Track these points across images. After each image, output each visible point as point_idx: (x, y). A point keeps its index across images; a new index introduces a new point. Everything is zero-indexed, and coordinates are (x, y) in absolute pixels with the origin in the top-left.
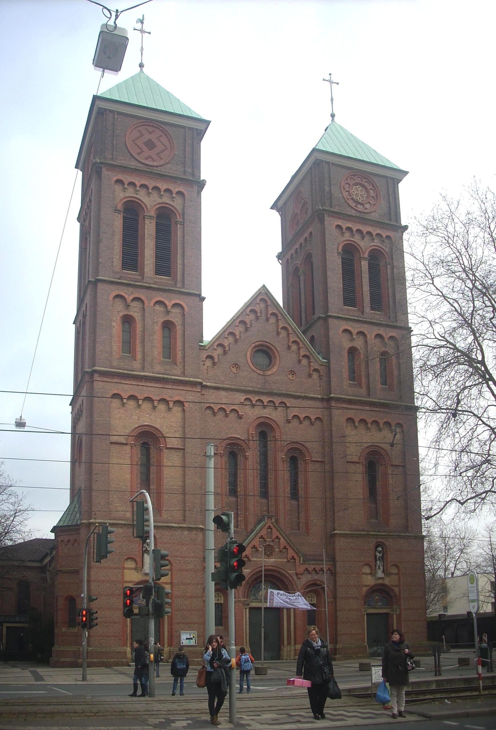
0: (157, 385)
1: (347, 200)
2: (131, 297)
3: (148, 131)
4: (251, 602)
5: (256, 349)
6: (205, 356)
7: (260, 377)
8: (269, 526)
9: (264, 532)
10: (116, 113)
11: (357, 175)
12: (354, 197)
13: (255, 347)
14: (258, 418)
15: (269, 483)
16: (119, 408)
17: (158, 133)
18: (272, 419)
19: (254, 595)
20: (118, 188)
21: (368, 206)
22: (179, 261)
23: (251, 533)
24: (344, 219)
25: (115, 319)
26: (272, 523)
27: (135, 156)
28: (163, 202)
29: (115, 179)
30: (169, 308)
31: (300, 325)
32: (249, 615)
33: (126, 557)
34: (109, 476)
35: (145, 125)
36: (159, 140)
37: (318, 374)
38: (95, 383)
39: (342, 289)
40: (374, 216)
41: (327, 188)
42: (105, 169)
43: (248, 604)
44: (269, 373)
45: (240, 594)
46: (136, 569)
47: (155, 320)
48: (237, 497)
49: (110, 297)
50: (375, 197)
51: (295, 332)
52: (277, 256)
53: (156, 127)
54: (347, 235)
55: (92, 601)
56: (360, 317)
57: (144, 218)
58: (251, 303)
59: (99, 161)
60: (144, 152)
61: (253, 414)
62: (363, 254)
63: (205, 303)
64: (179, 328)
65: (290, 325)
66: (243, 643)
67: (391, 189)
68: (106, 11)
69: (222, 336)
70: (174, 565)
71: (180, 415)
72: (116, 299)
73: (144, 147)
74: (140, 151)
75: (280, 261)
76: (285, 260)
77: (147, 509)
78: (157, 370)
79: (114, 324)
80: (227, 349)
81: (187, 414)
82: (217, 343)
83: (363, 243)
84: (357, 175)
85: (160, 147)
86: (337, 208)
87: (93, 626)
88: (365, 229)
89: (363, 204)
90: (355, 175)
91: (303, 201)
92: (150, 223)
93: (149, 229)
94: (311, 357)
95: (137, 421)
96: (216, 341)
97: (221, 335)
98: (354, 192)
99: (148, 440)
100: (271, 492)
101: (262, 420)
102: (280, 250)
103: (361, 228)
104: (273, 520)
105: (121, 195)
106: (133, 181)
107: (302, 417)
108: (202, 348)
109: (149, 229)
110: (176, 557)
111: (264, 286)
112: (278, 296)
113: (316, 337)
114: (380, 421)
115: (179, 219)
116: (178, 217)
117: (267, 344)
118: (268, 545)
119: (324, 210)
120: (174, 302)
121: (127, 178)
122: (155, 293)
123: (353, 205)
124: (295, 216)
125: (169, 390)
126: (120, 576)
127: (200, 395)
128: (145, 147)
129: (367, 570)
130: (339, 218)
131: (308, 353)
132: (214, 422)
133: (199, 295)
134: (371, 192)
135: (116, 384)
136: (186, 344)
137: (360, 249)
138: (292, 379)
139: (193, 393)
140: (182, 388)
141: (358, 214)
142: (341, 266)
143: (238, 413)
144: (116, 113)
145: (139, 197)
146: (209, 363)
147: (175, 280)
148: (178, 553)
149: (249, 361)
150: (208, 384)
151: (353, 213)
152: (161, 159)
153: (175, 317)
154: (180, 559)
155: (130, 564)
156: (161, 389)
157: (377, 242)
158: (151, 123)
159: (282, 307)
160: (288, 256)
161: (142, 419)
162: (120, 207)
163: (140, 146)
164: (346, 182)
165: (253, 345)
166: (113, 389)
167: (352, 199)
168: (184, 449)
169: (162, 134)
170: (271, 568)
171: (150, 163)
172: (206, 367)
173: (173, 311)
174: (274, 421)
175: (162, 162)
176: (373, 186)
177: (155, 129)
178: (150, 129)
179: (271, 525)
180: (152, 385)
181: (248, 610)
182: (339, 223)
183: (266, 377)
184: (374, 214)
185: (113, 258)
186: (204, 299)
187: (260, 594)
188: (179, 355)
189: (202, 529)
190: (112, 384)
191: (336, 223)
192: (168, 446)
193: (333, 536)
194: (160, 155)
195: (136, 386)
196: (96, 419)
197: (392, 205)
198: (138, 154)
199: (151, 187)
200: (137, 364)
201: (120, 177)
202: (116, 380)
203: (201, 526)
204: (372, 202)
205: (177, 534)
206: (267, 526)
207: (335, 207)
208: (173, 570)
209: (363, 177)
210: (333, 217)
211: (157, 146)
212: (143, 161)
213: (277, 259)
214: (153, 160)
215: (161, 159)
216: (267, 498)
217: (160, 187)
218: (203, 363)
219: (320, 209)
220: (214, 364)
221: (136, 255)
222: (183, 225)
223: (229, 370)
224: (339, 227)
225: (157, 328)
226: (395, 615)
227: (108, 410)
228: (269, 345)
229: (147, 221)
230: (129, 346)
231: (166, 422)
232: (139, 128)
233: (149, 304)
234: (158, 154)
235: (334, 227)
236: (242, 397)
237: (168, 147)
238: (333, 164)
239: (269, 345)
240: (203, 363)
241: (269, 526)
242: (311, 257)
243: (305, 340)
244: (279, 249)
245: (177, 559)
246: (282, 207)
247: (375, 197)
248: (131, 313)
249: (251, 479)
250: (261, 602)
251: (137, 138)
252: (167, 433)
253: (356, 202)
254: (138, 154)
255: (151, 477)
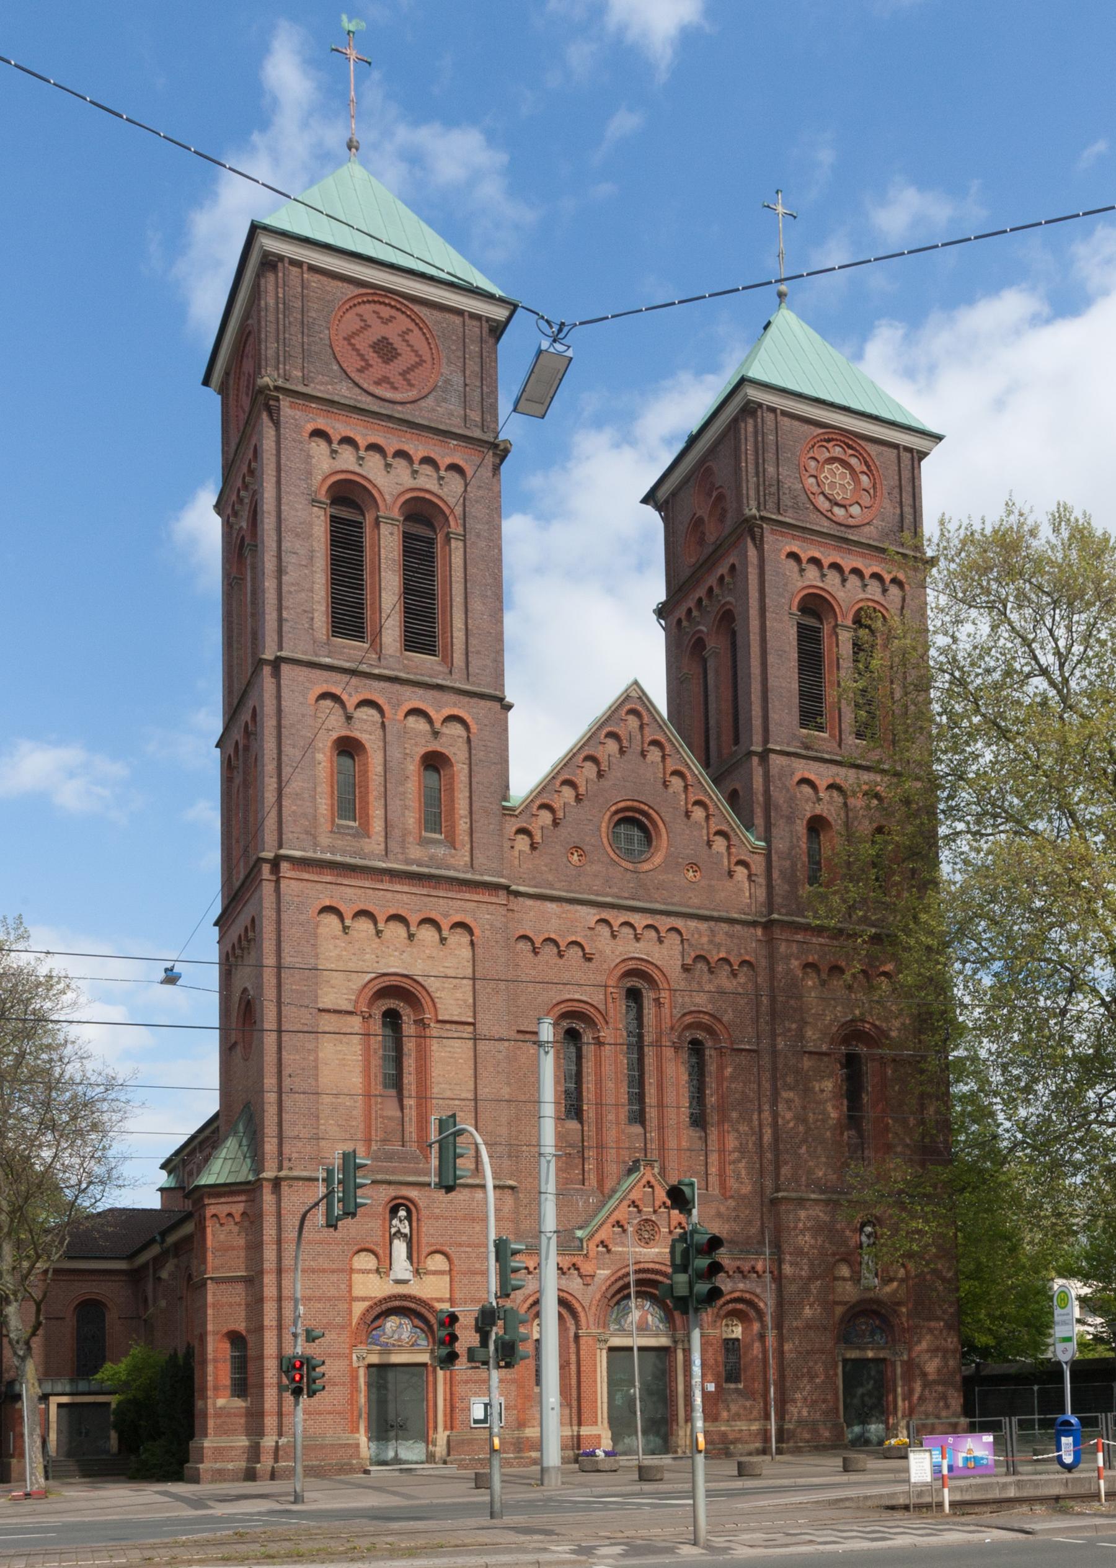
0: (414, 890)
1: (811, 496)
2: (355, 700)
3: (380, 318)
4: (612, 1335)
5: (620, 815)
6: (514, 829)
7: (629, 875)
8: (649, 1182)
9: (635, 1195)
10: (305, 268)
11: (833, 440)
12: (827, 491)
13: (616, 812)
14: (624, 961)
15: (647, 1095)
16: (335, 938)
17: (403, 322)
18: (652, 964)
19: (618, 1321)
20: (319, 448)
21: (855, 510)
22: (458, 623)
23: (610, 1197)
24: (804, 540)
25: (321, 745)
26: (654, 1175)
27: (352, 375)
28: (418, 486)
29: (310, 427)
30: (437, 725)
31: (707, 765)
32: (608, 1363)
33: (356, 1248)
34: (317, 1080)
35: (374, 302)
36: (404, 340)
37: (746, 871)
38: (283, 884)
39: (797, 692)
40: (867, 535)
41: (771, 470)
42: (287, 404)
43: (606, 1341)
44: (646, 867)
45: (591, 1319)
46: (377, 1271)
47: (408, 751)
48: (581, 1122)
49: (309, 696)
50: (872, 491)
51: (700, 782)
52: (654, 611)
53: (398, 309)
54: (812, 573)
55: (313, 1341)
56: (837, 754)
57: (377, 523)
58: (609, 717)
59: (271, 384)
60: (371, 366)
61: (616, 950)
62: (844, 617)
63: (511, 714)
64: (460, 770)
65: (689, 768)
66: (596, 1418)
67: (906, 474)
68: (542, 323)
69: (549, 787)
70: (456, 1262)
71: (466, 953)
72: (321, 702)
73: (371, 356)
74: (363, 364)
75: (663, 622)
76: (674, 619)
77: (775, 1385)
78: (416, 856)
79: (320, 756)
80: (560, 814)
81: (479, 951)
82: (538, 803)
83: (842, 594)
84: (833, 440)
85: (407, 358)
86: (790, 513)
87: (314, 1393)
88: (848, 562)
89: (844, 506)
90: (829, 441)
91: (715, 494)
92: (391, 534)
93: (387, 547)
94: (732, 834)
95: (376, 965)
96: (536, 797)
97: (546, 786)
98: (826, 478)
99: (396, 1005)
100: (652, 1113)
101: (632, 965)
102: (663, 598)
103: (839, 561)
104: (656, 1170)
105: (325, 465)
106: (352, 435)
107: (714, 957)
108: (508, 812)
109: (387, 547)
110: (460, 1245)
111: (636, 683)
112: (659, 698)
113: (741, 794)
114: (342, 908)
115: (455, 527)
116: (452, 523)
117: (642, 806)
118: (646, 1220)
119: (762, 518)
120: (447, 712)
121: (338, 427)
122: (407, 691)
123: (822, 503)
124: (697, 523)
125: (441, 901)
126: (343, 1286)
127: (504, 912)
128: (375, 355)
129: (845, 1271)
130: (794, 537)
131: (725, 828)
132: (534, 968)
133: (501, 700)
134: (864, 479)
135: (329, 886)
136: (474, 805)
137: (836, 607)
138: (694, 880)
139: (492, 908)
140: (467, 896)
141: (835, 530)
142: (795, 643)
143: (583, 949)
144: (305, 268)
145: (364, 473)
146: (523, 842)
147: (448, 660)
148: (464, 1238)
149: (605, 840)
150: (522, 889)
151: (825, 526)
152: (411, 385)
153: (452, 741)
154: (468, 1249)
155: (366, 1261)
156: (423, 898)
157: (874, 590)
158: (386, 296)
159: (665, 716)
160: (681, 612)
161: (384, 961)
162: (322, 496)
163: (362, 352)
164: (811, 454)
165: (613, 808)
166: (321, 896)
167: (822, 493)
168: (473, 1024)
169: (412, 326)
170: (651, 1266)
171: (389, 395)
172: (516, 854)
173: (445, 730)
174: (657, 966)
175: (412, 394)
176: (868, 467)
177: (393, 312)
178: (386, 312)
179: (652, 1180)
180: (406, 889)
181: (604, 1352)
182: (795, 549)
183: (641, 876)
184: (866, 529)
185: (312, 611)
186: (509, 707)
187: (629, 1319)
188: (463, 825)
189: (512, 1188)
190: (319, 886)
191: (788, 549)
192: (440, 1018)
193: (774, 1202)
194: (408, 376)
195: (371, 891)
196: (289, 959)
197: (907, 510)
198: (359, 370)
199: (390, 451)
200: (374, 844)
201: (321, 423)
202: (329, 879)
203: (511, 1183)
204: (866, 500)
205: (462, 1198)
206: (644, 1181)
207: (785, 511)
208: (454, 1273)
209: (846, 444)
210: (782, 534)
211: (400, 355)
212: (373, 389)
213: (655, 617)
214: (396, 389)
215: (411, 385)
216: (580, 1120)
217: (411, 453)
218: (509, 844)
219: (754, 517)
220: (533, 847)
221: (361, 606)
222: (464, 541)
223: (565, 860)
224: (793, 555)
225: (412, 767)
226: (898, 1363)
227: (312, 942)
228: (646, 808)
229: (385, 529)
230: (350, 802)
231: (438, 966)
232: (360, 309)
233: (395, 715)
234: (404, 374)
235: (783, 557)
236: (590, 915)
237: (427, 356)
238: (784, 413)
239: (646, 808)
240: (509, 844)
241: (649, 1182)
242: (733, 620)
243: (719, 800)
244: (660, 595)
245: (463, 1249)
246: (667, 502)
247: (872, 491)
248: (356, 734)
249: (610, 1085)
250: (631, 1335)
251: (355, 334)
252: (438, 990)
253: (830, 500)
254: (359, 370)
255: (405, 1081)
